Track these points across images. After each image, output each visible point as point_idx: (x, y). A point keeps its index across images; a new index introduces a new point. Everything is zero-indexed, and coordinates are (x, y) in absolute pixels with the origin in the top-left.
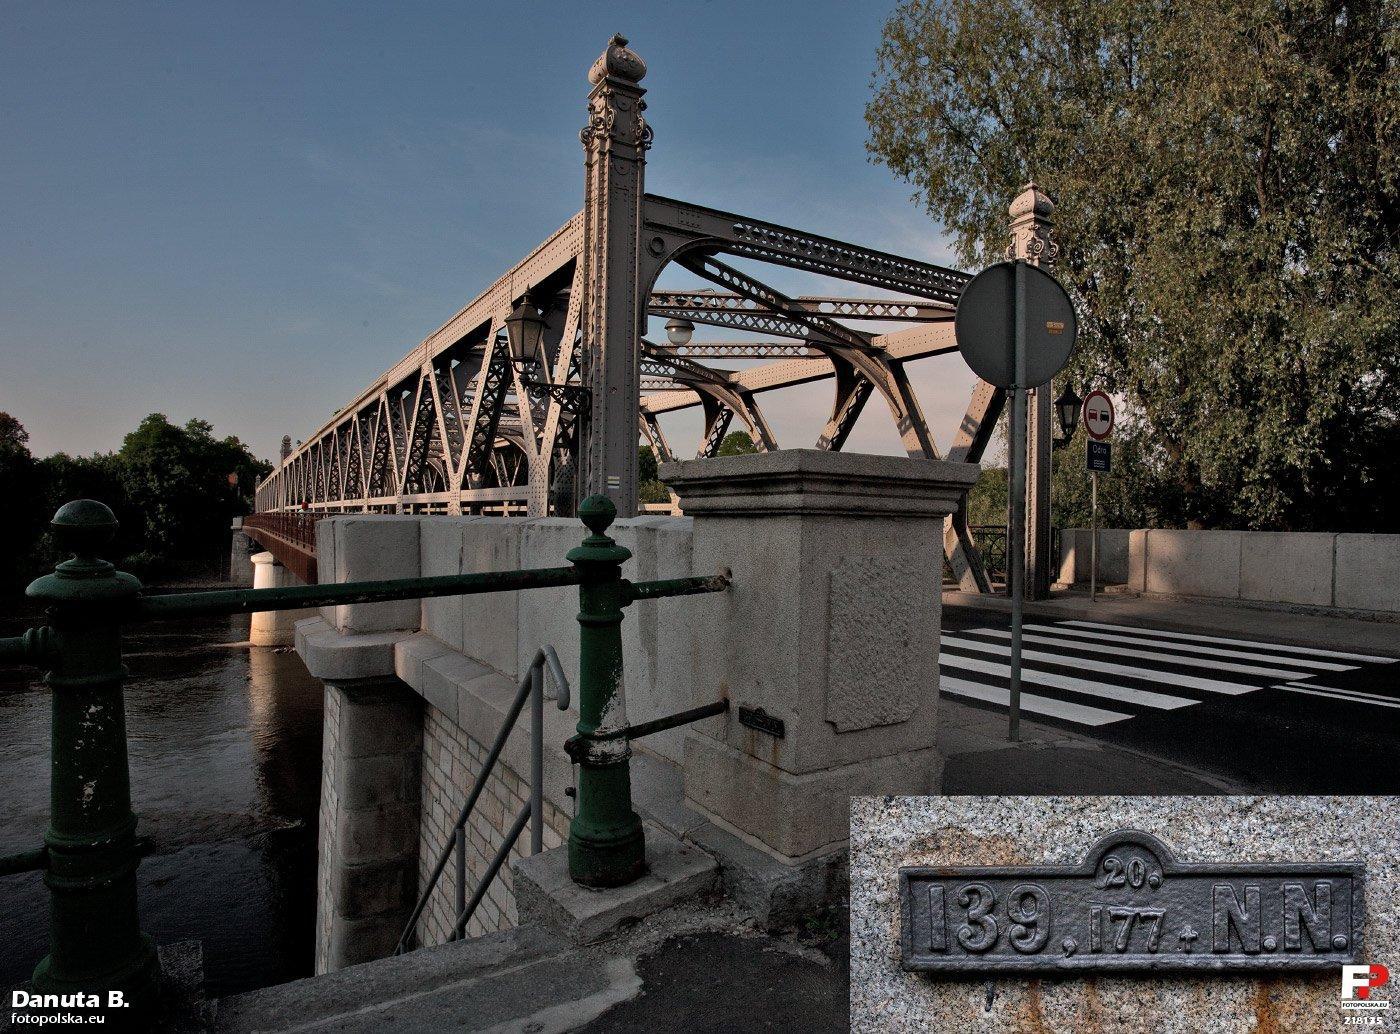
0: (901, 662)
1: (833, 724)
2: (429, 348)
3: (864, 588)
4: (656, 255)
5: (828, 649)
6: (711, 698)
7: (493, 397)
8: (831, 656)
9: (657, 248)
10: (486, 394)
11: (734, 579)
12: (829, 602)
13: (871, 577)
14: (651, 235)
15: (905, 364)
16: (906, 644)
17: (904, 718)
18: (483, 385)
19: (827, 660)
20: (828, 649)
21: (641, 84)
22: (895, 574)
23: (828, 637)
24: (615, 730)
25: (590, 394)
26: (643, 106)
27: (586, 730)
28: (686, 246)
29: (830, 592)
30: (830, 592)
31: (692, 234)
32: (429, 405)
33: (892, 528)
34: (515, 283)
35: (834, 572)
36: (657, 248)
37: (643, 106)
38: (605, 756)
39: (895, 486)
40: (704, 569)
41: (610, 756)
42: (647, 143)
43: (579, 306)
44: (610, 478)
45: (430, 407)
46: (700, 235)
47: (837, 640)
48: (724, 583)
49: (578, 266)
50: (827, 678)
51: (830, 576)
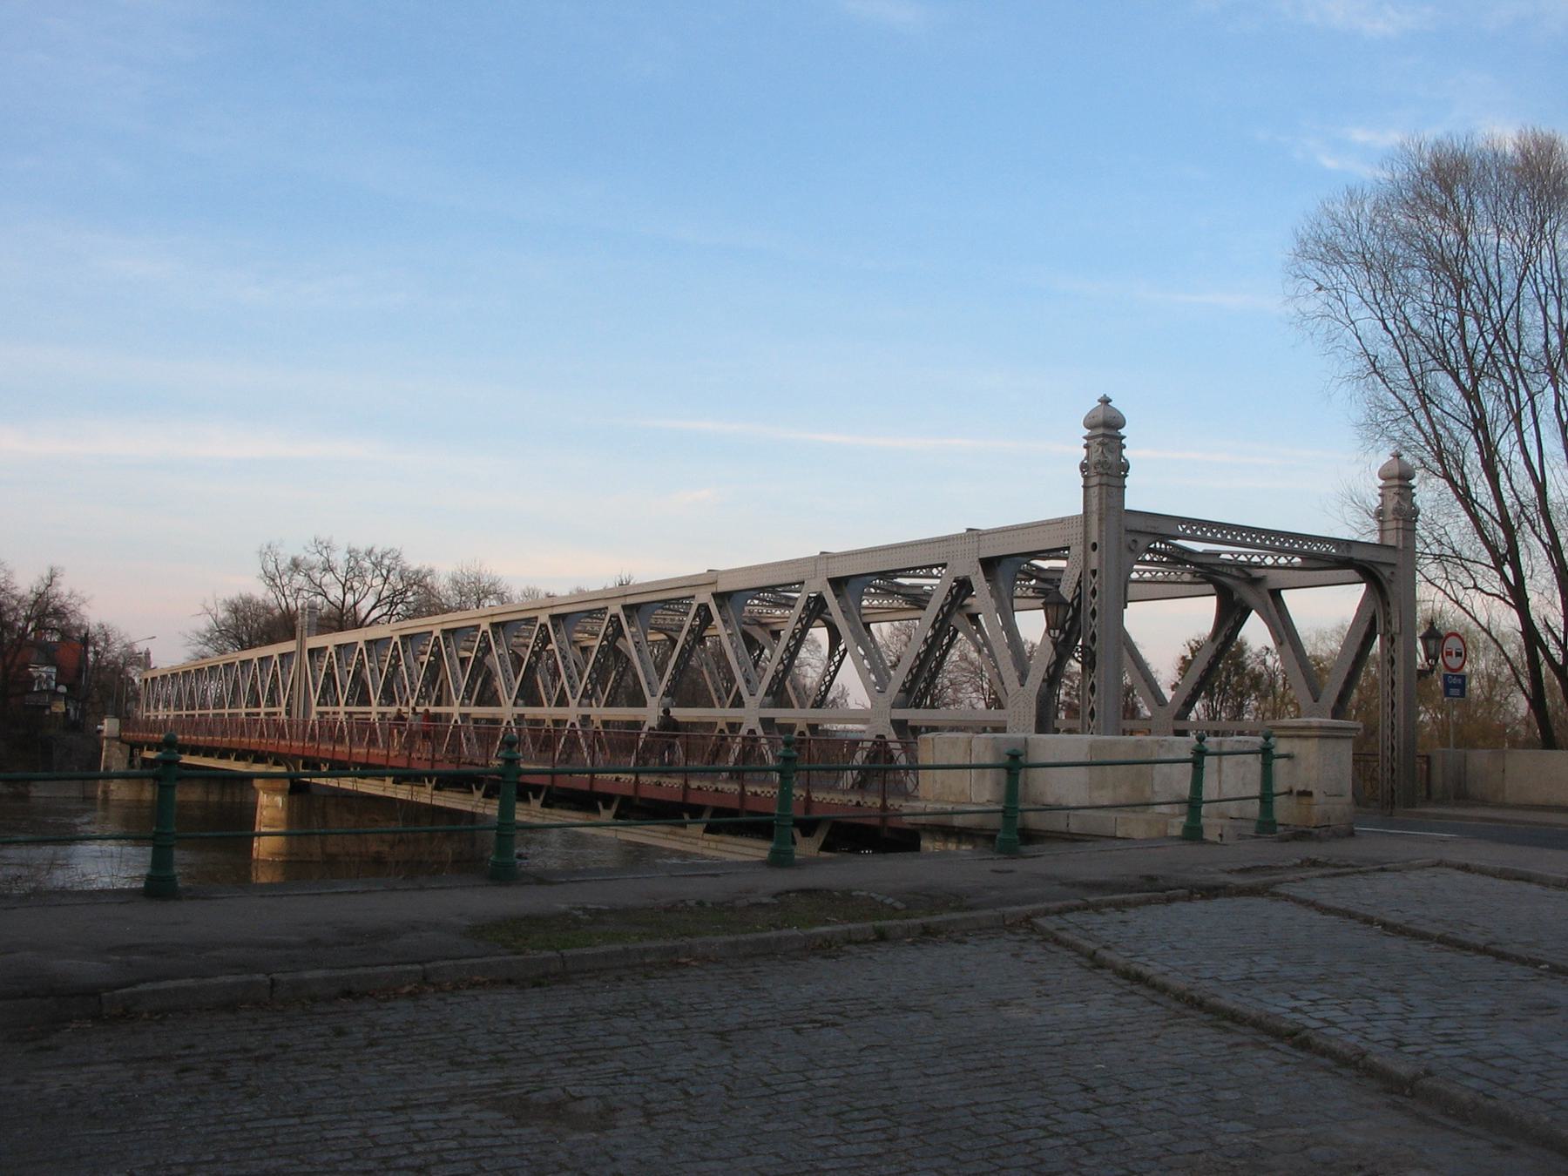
4: (1132, 550)
14: (1130, 538)
21: (1122, 432)
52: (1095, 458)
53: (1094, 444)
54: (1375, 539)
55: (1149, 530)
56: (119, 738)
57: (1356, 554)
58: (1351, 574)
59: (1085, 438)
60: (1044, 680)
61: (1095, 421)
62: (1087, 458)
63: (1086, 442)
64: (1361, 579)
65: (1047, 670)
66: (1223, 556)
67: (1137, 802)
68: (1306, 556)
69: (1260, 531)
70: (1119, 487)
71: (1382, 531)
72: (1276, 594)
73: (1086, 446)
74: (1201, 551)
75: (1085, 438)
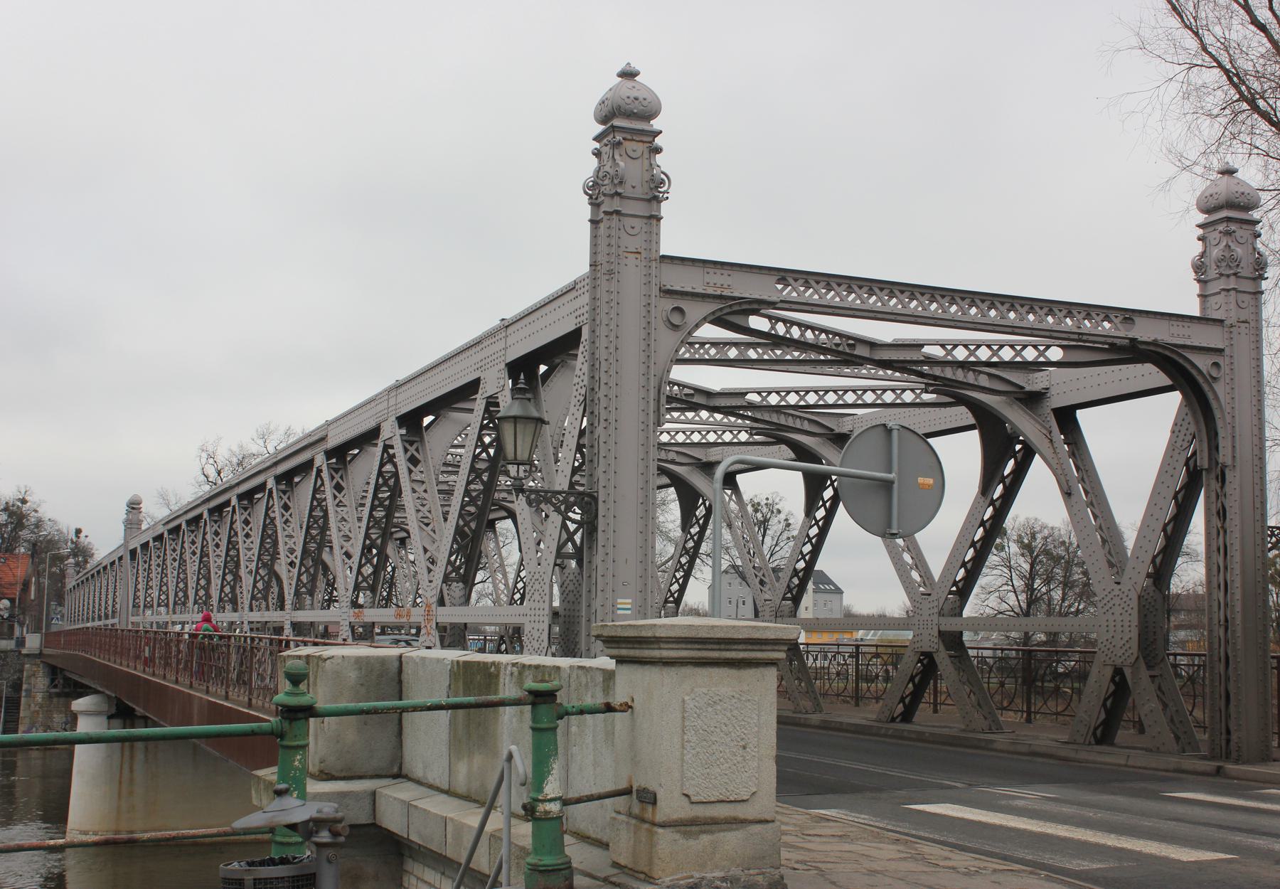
0: (739, 759)
1: (687, 796)
2: (392, 402)
3: (710, 709)
4: (675, 327)
5: (683, 747)
6: (623, 785)
7: (488, 454)
8: (685, 752)
9: (676, 319)
10: (478, 451)
11: (635, 705)
12: (683, 717)
13: (715, 702)
14: (669, 304)
15: (1081, 415)
16: (744, 748)
17: (745, 798)
18: (468, 466)
19: (683, 754)
20: (683, 747)
21: (656, 124)
22: (734, 701)
23: (683, 739)
24: (553, 796)
25: (596, 499)
26: (658, 150)
27: (534, 795)
28: (721, 309)
29: (684, 711)
30: (684, 711)
31: (721, 297)
32: (390, 478)
33: (733, 672)
34: (510, 341)
35: (686, 698)
36: (676, 319)
37: (658, 150)
38: (547, 812)
39: (736, 643)
40: (619, 698)
41: (550, 812)
42: (664, 193)
43: (584, 389)
44: (619, 601)
45: (391, 482)
46: (734, 298)
47: (689, 741)
48: (627, 707)
49: (583, 339)
50: (682, 766)
51: (683, 701)
52: (1216, 253)
53: (1214, 236)
54: (1192, 307)
55: (710, 291)
56: (40, 655)
57: (1144, 332)
58: (1150, 374)
59: (1199, 226)
60: (1148, 575)
61: (1212, 203)
62: (1203, 255)
63: (1200, 232)
64: (1167, 382)
65: (1153, 561)
66: (926, 349)
67: (708, 805)
68: (1074, 342)
69: (1032, 304)
70: (1255, 293)
71: (1203, 296)
72: (1066, 419)
73: (597, 154)
74: (889, 340)
75: (1199, 226)
